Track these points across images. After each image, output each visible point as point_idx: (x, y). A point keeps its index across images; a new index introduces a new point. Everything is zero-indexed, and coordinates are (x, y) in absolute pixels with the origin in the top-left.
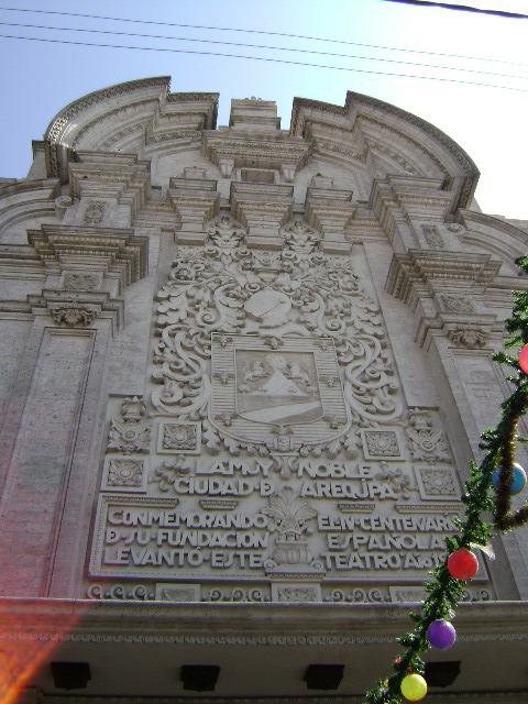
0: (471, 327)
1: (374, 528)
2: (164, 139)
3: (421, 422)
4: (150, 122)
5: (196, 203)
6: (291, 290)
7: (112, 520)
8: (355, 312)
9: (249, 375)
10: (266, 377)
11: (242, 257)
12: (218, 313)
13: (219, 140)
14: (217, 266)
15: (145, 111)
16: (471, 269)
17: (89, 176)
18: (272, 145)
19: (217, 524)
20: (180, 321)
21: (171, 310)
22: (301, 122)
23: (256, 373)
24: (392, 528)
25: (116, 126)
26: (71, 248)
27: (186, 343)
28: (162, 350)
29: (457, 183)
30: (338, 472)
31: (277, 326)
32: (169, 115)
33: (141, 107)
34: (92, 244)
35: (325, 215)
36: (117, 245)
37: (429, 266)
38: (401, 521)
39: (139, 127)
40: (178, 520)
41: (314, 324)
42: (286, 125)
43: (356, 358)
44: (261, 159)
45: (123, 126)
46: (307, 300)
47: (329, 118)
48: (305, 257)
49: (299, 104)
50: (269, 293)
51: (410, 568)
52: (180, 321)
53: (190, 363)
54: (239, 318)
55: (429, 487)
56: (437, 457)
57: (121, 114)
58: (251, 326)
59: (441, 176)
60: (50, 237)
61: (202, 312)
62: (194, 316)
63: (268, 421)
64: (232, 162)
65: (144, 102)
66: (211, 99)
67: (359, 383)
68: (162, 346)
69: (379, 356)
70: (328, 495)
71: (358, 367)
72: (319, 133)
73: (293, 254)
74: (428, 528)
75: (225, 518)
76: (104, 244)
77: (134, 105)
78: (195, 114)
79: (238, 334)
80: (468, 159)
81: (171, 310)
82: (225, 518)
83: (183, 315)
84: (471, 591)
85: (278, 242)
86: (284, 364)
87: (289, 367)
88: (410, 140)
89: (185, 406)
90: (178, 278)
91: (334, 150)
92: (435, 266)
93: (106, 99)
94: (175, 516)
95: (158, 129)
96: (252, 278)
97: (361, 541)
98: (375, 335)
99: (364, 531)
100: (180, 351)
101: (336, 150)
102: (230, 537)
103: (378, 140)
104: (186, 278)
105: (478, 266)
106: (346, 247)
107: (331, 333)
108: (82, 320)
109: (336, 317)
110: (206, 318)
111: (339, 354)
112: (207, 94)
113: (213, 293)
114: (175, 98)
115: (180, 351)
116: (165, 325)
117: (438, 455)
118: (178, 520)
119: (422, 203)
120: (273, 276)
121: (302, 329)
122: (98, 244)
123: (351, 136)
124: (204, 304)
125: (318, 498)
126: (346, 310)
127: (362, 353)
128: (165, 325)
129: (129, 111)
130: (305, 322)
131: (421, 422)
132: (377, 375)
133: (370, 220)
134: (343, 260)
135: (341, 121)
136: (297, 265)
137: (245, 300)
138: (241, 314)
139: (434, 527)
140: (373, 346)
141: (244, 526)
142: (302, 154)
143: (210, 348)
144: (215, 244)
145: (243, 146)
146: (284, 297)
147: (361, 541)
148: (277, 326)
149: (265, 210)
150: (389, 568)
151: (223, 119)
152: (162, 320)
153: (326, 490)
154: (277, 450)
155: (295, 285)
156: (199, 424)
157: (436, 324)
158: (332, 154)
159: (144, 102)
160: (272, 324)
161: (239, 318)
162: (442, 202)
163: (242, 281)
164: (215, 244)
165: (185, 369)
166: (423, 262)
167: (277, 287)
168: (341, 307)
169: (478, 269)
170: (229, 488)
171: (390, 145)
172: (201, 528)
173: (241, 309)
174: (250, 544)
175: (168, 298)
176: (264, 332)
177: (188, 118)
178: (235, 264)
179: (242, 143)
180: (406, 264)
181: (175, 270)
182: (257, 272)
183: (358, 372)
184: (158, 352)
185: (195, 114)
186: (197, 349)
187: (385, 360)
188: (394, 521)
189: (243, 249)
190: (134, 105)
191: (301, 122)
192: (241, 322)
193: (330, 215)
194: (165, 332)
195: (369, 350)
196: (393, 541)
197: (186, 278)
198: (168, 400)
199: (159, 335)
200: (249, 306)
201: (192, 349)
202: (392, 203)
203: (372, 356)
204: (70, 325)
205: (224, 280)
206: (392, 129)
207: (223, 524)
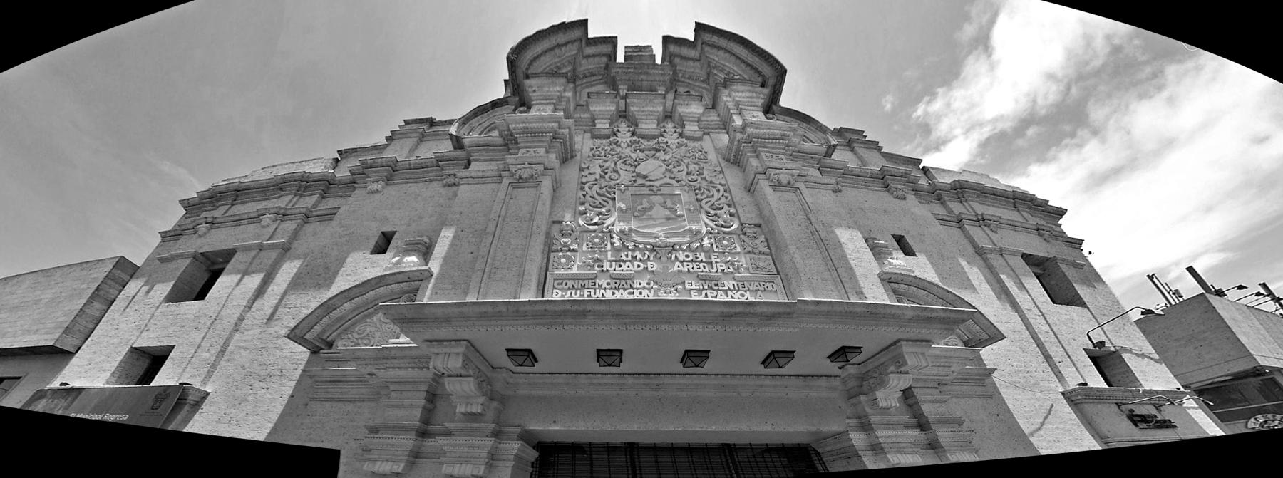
1: (720, 288)
2: (585, 77)
3: (750, 231)
4: (574, 62)
6: (665, 160)
7: (556, 286)
8: (705, 172)
9: (639, 207)
10: (651, 208)
11: (633, 144)
12: (619, 175)
13: (618, 70)
14: (618, 150)
19: (621, 286)
20: (596, 180)
21: (590, 174)
22: (668, 54)
23: (644, 206)
24: (732, 288)
25: (554, 61)
27: (599, 191)
28: (584, 196)
29: (771, 82)
30: (697, 258)
31: (657, 180)
32: (588, 56)
38: (738, 285)
40: (597, 285)
41: (680, 179)
42: (658, 60)
43: (708, 197)
45: (559, 62)
46: (675, 165)
47: (685, 51)
48: (673, 141)
49: (667, 40)
50: (651, 161)
52: (596, 180)
53: (602, 202)
54: (633, 177)
55: (755, 267)
56: (760, 251)
57: (557, 51)
58: (640, 181)
59: (760, 79)
61: (609, 174)
62: (604, 177)
64: (626, 87)
66: (612, 41)
67: (709, 210)
68: (584, 193)
69: (723, 195)
70: (691, 270)
72: (681, 65)
73: (666, 140)
75: (626, 283)
79: (632, 185)
80: (777, 62)
81: (590, 174)
82: (626, 283)
83: (598, 177)
85: (657, 132)
86: (662, 201)
87: (665, 202)
88: (738, 57)
90: (594, 156)
91: (688, 78)
94: (595, 283)
95: (583, 68)
96: (642, 155)
97: (712, 295)
98: (720, 184)
99: (714, 290)
100: (596, 196)
101: (690, 78)
102: (629, 293)
103: (716, 61)
104: (599, 156)
106: (699, 134)
107: (692, 183)
109: (694, 175)
110: (612, 177)
111: (696, 195)
112: (610, 37)
113: (615, 164)
114: (591, 41)
115: (596, 196)
116: (587, 182)
117: (760, 249)
118: (597, 285)
120: (653, 152)
121: (674, 182)
123: (697, 64)
124: (611, 169)
125: (685, 273)
126: (701, 171)
127: (711, 194)
128: (587, 182)
130: (674, 178)
131: (750, 231)
132: (721, 206)
134: (697, 144)
135: (693, 53)
136: (669, 146)
137: (636, 166)
138: (635, 174)
139: (759, 287)
140: (718, 191)
141: (639, 286)
143: (614, 193)
144: (617, 137)
146: (660, 163)
147: (712, 295)
148: (657, 180)
151: (620, 58)
152: (584, 180)
153: (690, 268)
154: (659, 247)
155: (667, 157)
156: (609, 234)
158: (687, 81)
160: (653, 179)
161: (633, 177)
162: (762, 96)
163: (634, 156)
164: (617, 137)
165: (599, 206)
167: (657, 159)
168: (697, 169)
170: (628, 267)
171: (724, 65)
172: (611, 289)
173: (634, 172)
174: (641, 286)
175: (588, 168)
176: (648, 183)
178: (630, 148)
181: (593, 152)
182: (642, 151)
183: (709, 204)
184: (582, 197)
186: (607, 194)
187: (727, 198)
188: (734, 285)
189: (635, 138)
191: (668, 54)
192: (634, 179)
194: (587, 186)
195: (716, 193)
196: (733, 295)
197: (599, 156)
198: (589, 223)
199: (582, 189)
200: (638, 169)
201: (604, 195)
203: (717, 196)
205: (623, 156)
206: (727, 51)
207: (625, 286)
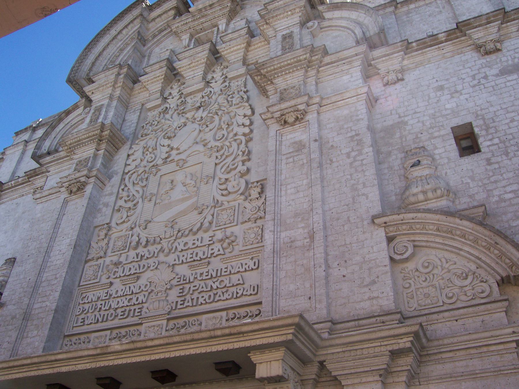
0: (290, 110)
2: (155, 36)
5: (155, 79)
15: (135, 26)
16: (300, 61)
17: (94, 91)
18: (209, 12)
25: (118, 46)
26: (78, 145)
33: (131, 25)
34: (85, 139)
35: (229, 53)
36: (96, 134)
37: (271, 71)
39: (132, 39)
44: (205, 25)
51: (218, 301)
57: (119, 37)
60: (262, 71)
63: (165, 220)
65: (132, 22)
71: (226, 163)
74: (237, 270)
76: (91, 137)
77: (126, 27)
78: (169, 10)
84: (284, 301)
89: (127, 222)
91: (153, 38)
92: (275, 69)
93: (108, 32)
105: (305, 56)
108: (297, 119)
119: (283, 18)
122: (88, 137)
129: (124, 32)
133: (260, 42)
142: (228, 9)
145: (192, 21)
149: (193, 67)
150: (206, 303)
157: (269, 115)
159: (132, 22)
166: (265, 70)
169: (305, 59)
177: (165, 15)
179: (190, 20)
180: (257, 76)
185: (169, 10)
190: (126, 27)
193: (232, 52)
202: (265, 27)
204: (293, 124)
